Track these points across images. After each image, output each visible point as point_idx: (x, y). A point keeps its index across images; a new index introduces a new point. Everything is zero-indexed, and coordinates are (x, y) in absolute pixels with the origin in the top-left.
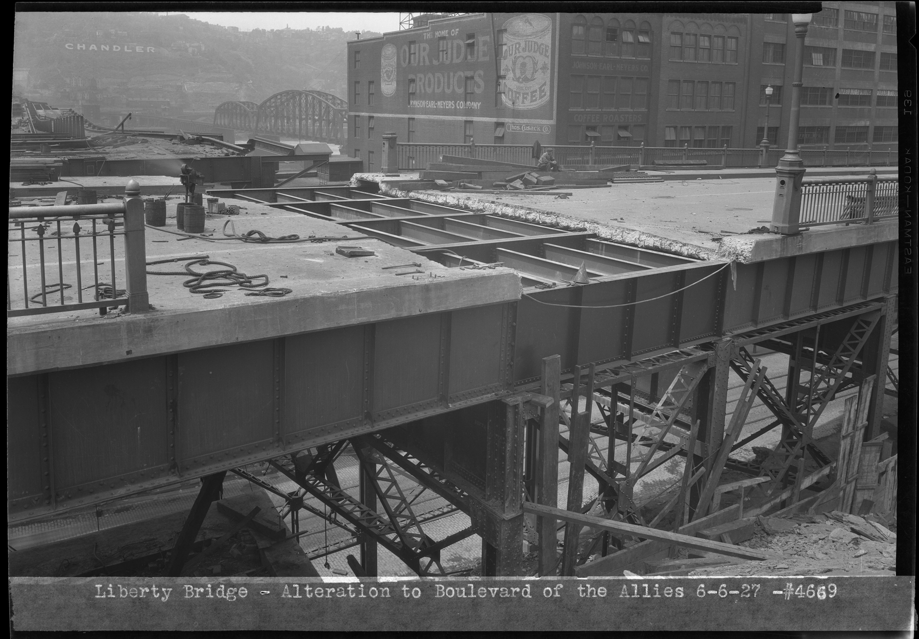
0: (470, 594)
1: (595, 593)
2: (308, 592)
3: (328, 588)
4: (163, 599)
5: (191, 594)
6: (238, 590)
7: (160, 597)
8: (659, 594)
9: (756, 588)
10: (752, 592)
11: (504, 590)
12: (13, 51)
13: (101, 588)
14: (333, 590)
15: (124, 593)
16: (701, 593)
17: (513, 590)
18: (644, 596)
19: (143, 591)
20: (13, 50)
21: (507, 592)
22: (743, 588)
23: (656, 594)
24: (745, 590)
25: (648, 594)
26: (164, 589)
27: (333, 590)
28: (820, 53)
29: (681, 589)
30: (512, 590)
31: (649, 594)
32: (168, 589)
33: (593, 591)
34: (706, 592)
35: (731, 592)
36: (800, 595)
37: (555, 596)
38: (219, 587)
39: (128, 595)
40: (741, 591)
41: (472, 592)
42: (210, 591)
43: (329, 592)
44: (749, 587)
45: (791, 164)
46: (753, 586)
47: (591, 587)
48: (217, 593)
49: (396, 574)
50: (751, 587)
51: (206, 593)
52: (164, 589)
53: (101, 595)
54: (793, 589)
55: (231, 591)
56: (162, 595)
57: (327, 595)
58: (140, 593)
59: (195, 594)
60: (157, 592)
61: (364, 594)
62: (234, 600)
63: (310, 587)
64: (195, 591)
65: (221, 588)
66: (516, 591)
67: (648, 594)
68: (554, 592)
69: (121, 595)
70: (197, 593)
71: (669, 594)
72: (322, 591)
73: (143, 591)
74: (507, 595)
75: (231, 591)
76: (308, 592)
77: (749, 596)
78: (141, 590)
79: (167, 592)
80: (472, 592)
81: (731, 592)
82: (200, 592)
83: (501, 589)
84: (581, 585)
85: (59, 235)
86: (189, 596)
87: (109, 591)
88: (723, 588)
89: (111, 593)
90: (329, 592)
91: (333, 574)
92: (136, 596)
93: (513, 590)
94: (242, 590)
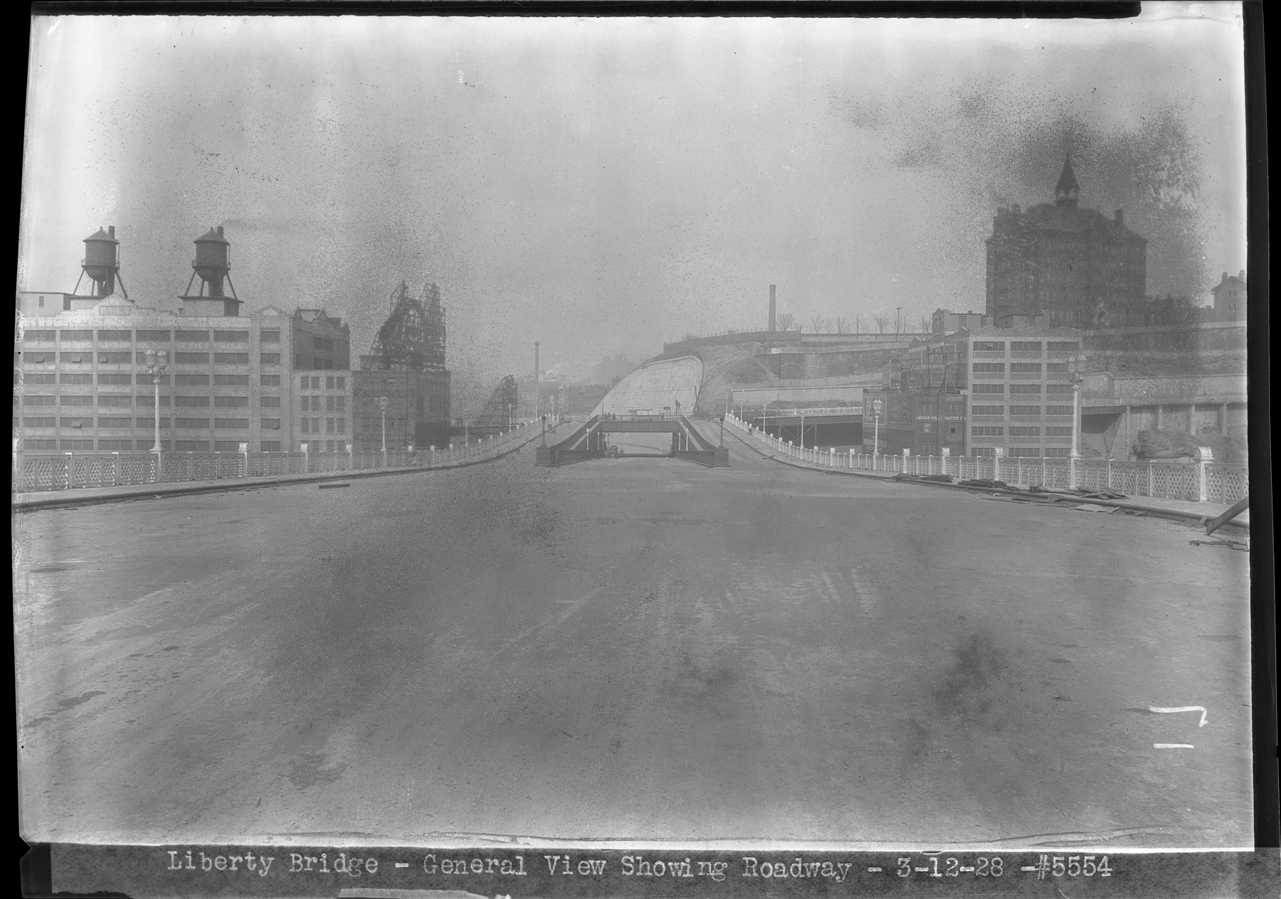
0: (463, 871)
1: (649, 868)
3: (555, 855)
4: (261, 871)
5: (717, 867)
6: (365, 861)
7: (257, 870)
11: (828, 866)
13: (273, 861)
14: (496, 862)
15: (207, 864)
17: (234, 860)
21: (784, 870)
24: (950, 866)
25: (938, 873)
27: (496, 862)
28: (942, 450)
30: (231, 860)
32: (847, 865)
33: (707, 866)
36: (1104, 872)
37: (455, 873)
39: (213, 866)
41: (936, 869)
45: (551, 415)
47: (908, 864)
48: (178, 868)
49: (357, 834)
56: (260, 866)
58: (229, 864)
61: (327, 868)
64: (305, 862)
65: (341, 858)
67: (938, 873)
68: (305, 862)
70: (233, 865)
72: (225, 862)
80: (936, 869)
83: (824, 866)
84: (249, 853)
85: (147, 401)
86: (295, 869)
89: (325, 865)
90: (491, 863)
93: (234, 860)
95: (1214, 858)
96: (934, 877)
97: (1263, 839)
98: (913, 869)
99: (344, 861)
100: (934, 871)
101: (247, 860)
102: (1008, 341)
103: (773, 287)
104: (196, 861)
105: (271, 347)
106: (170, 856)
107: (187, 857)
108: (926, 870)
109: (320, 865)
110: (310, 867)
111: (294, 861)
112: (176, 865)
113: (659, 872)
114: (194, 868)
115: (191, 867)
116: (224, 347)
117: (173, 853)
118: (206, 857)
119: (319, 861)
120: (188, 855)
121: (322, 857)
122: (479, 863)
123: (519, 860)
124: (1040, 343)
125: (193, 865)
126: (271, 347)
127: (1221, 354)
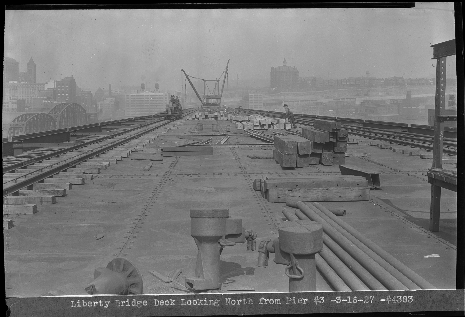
2: (244, 302)
4: (105, 307)
6: (143, 302)
7: (103, 306)
8: (295, 302)
9: (372, 298)
10: (370, 300)
12: (437, 1)
13: (73, 302)
15: (85, 304)
16: (399, 300)
17: (95, 303)
18: (265, 304)
19: (122, 302)
20: (4, 40)
22: (365, 298)
23: (205, 303)
24: (366, 299)
26: (105, 302)
29: (411, 297)
31: (80, 305)
32: (108, 302)
34: (358, 300)
35: (359, 300)
38: (133, 301)
40: (364, 299)
42: (350, 299)
43: (95, 304)
44: (368, 297)
46: (371, 297)
47: (250, 299)
50: (369, 297)
51: (292, 301)
52: (105, 302)
53: (74, 306)
54: (390, 299)
55: (216, 301)
57: (171, 304)
59: (121, 304)
60: (102, 303)
62: (353, 302)
63: (245, 299)
64: (121, 303)
65: (134, 301)
66: (306, 300)
67: (80, 305)
69: (132, 305)
70: (266, 302)
71: (162, 304)
73: (122, 302)
74: (206, 304)
75: (139, 303)
76: (244, 302)
77: (368, 302)
78: (94, 303)
79: (107, 303)
81: (359, 300)
82: (267, 301)
87: (78, 303)
88: (355, 298)
91: (228, 291)
92: (91, 306)
93: (95, 303)
94: (145, 302)
95: (58, 299)
96: (155, 306)
97: (459, 285)
98: (341, 300)
99: (135, 302)
100: (155, 304)
101: (100, 303)
102: (254, 95)
103: (237, 75)
104: (81, 304)
105: (166, 97)
106: (155, 301)
107: (77, 302)
108: (346, 300)
109: (127, 303)
110: (305, 302)
111: (117, 303)
112: (74, 306)
113: (195, 304)
114: (130, 305)
115: (79, 306)
116: (160, 97)
117: (73, 301)
118: (84, 301)
119: (126, 302)
120: (127, 301)
121: (293, 298)
122: (162, 302)
123: (349, 298)
124: (253, 95)
125: (129, 305)
126: (166, 97)
127: (450, 101)
